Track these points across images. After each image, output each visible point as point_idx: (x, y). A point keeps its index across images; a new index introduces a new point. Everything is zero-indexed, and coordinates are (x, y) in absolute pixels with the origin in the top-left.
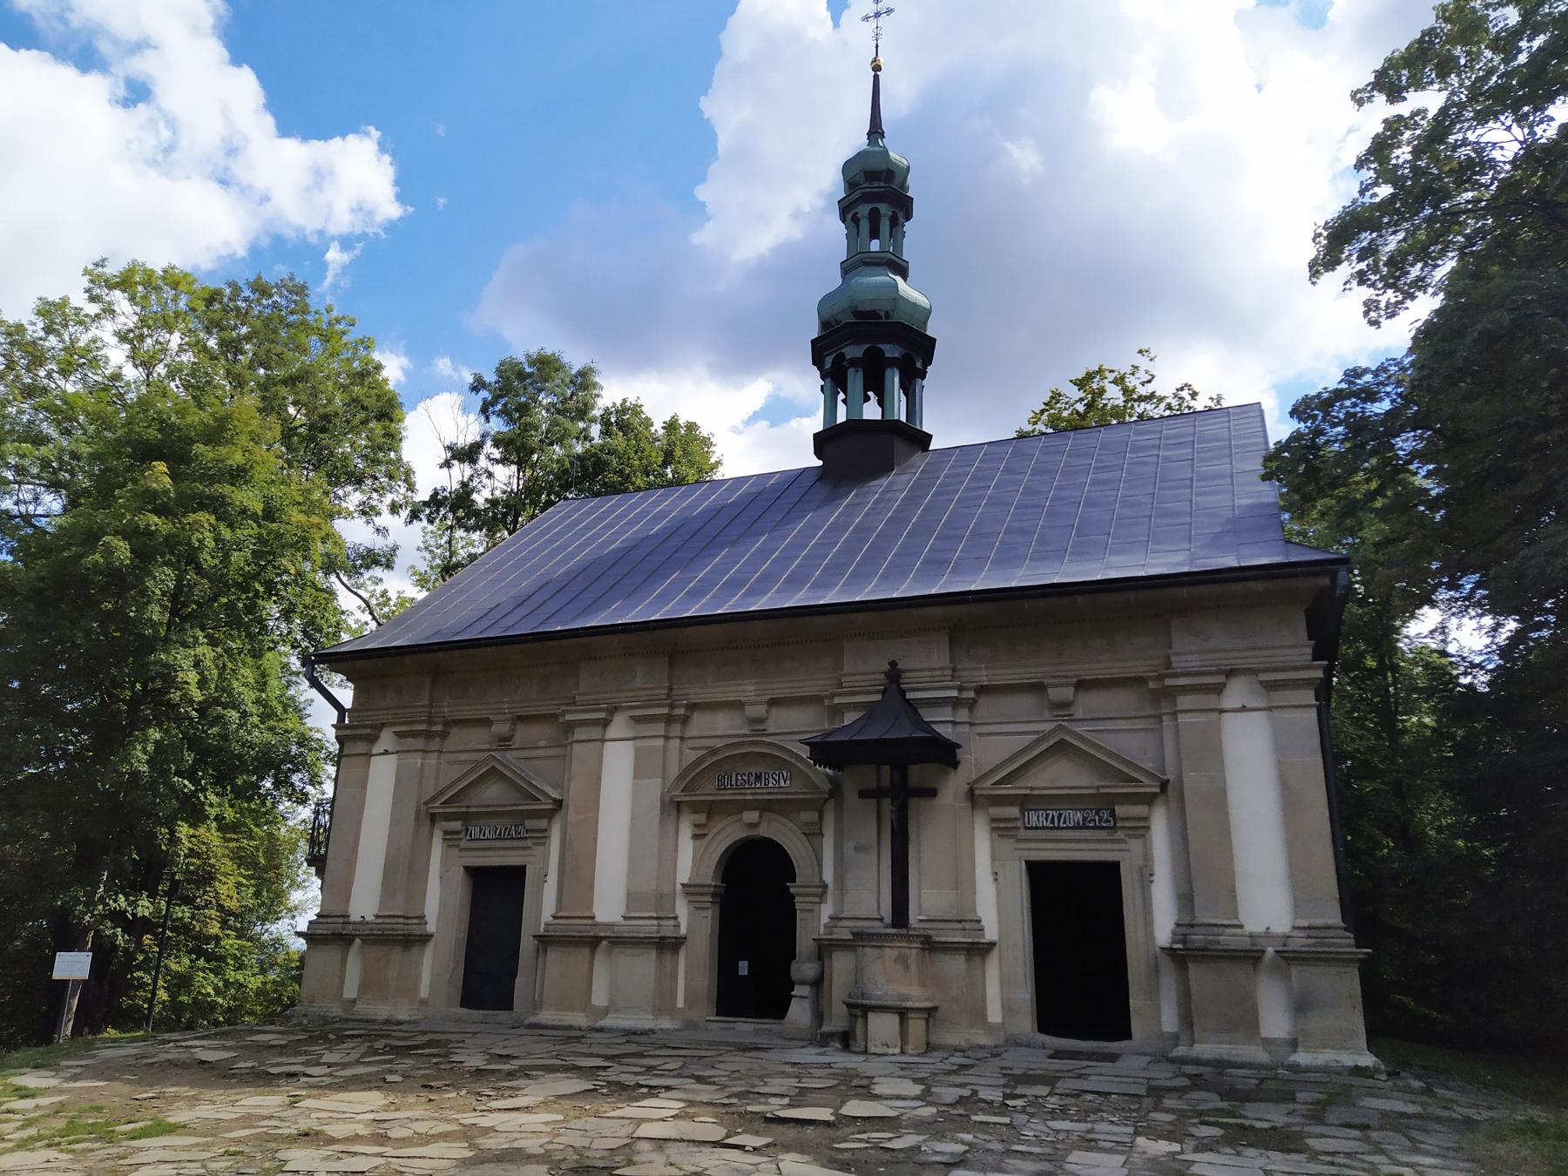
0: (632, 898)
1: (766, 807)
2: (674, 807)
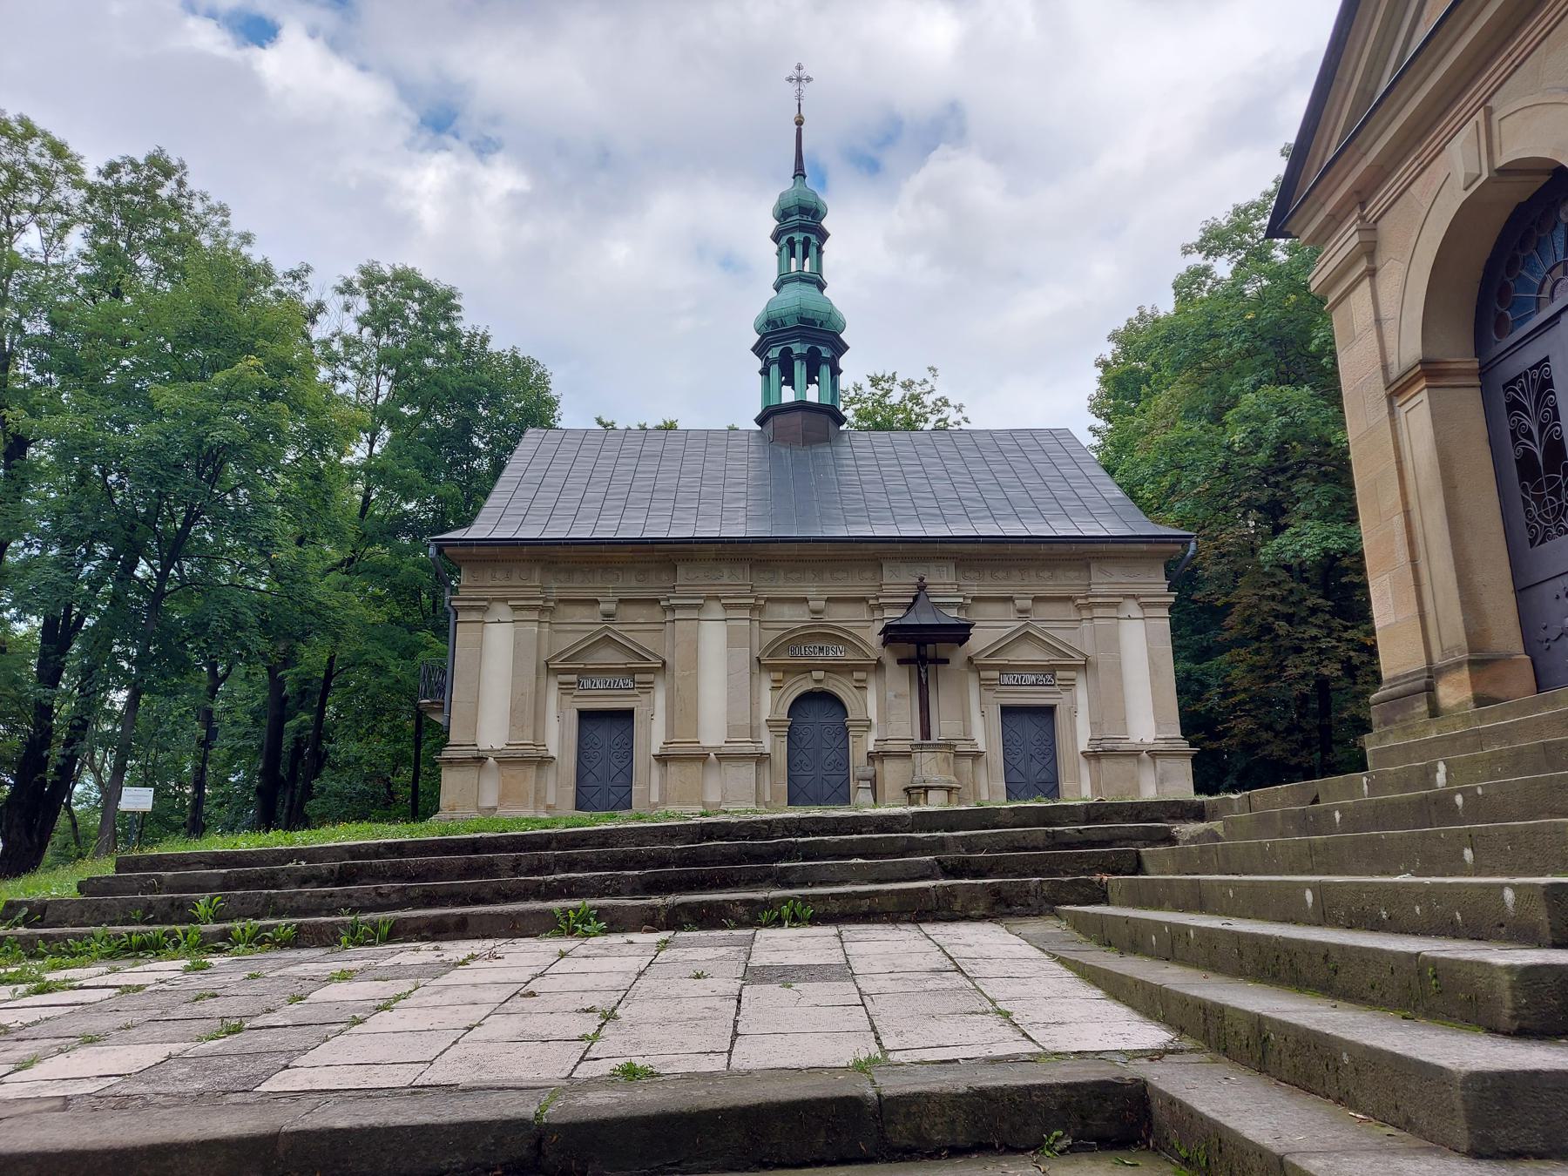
0: (731, 729)
1: (830, 669)
2: (760, 665)
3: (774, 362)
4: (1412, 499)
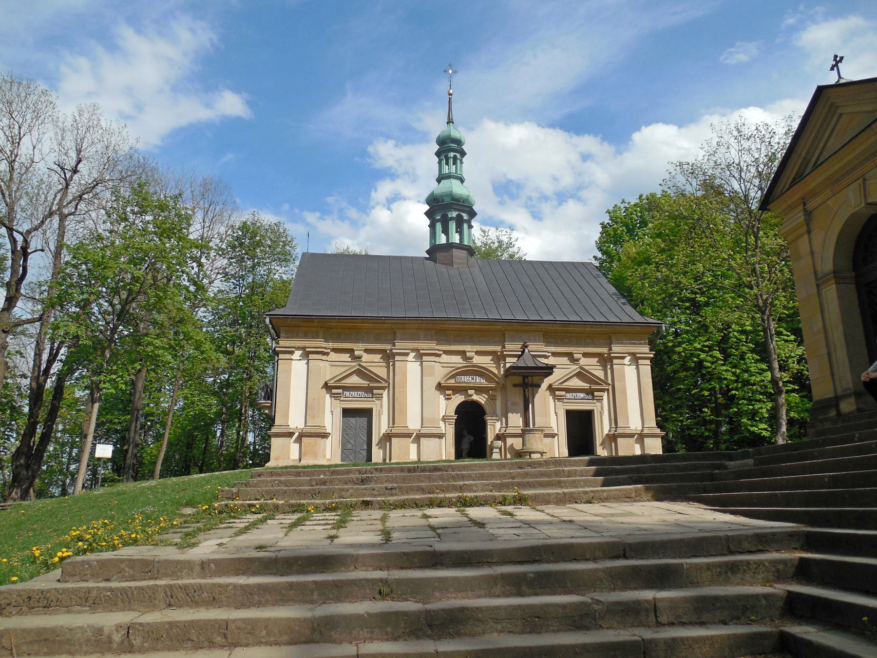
3: (438, 221)
4: (828, 327)
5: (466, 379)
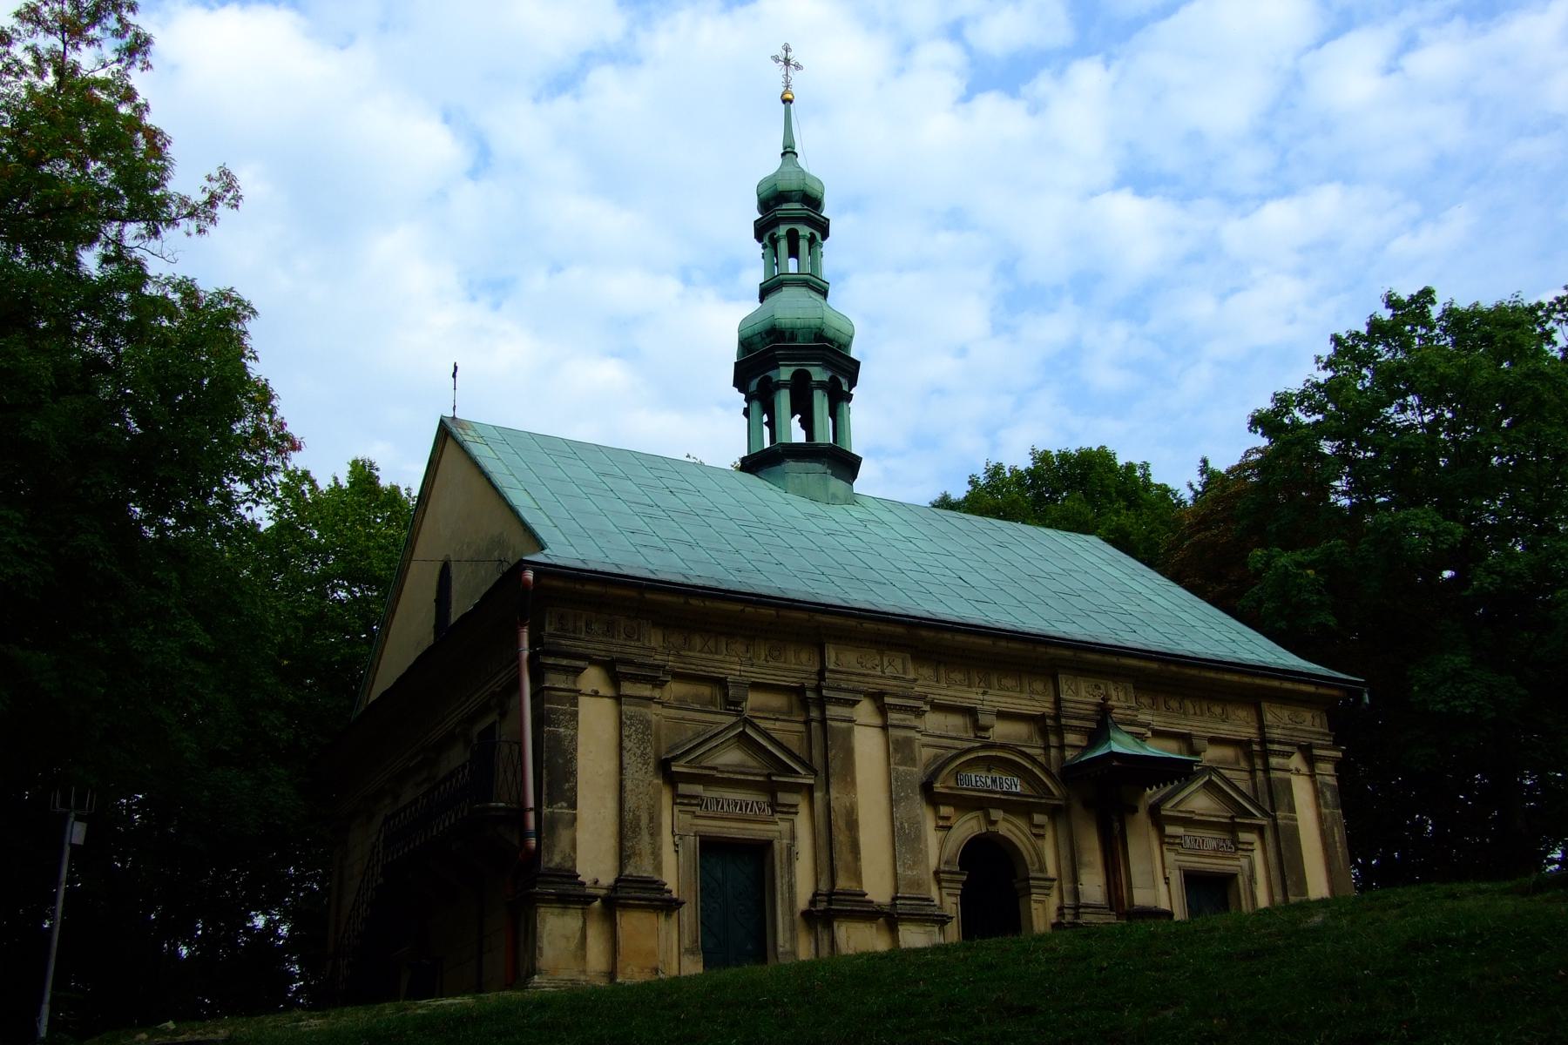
5: (980, 779)
